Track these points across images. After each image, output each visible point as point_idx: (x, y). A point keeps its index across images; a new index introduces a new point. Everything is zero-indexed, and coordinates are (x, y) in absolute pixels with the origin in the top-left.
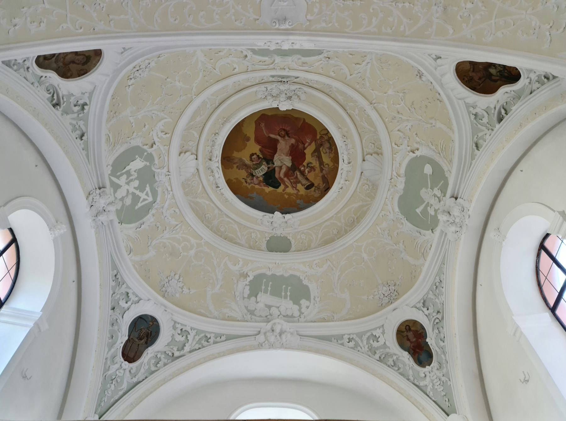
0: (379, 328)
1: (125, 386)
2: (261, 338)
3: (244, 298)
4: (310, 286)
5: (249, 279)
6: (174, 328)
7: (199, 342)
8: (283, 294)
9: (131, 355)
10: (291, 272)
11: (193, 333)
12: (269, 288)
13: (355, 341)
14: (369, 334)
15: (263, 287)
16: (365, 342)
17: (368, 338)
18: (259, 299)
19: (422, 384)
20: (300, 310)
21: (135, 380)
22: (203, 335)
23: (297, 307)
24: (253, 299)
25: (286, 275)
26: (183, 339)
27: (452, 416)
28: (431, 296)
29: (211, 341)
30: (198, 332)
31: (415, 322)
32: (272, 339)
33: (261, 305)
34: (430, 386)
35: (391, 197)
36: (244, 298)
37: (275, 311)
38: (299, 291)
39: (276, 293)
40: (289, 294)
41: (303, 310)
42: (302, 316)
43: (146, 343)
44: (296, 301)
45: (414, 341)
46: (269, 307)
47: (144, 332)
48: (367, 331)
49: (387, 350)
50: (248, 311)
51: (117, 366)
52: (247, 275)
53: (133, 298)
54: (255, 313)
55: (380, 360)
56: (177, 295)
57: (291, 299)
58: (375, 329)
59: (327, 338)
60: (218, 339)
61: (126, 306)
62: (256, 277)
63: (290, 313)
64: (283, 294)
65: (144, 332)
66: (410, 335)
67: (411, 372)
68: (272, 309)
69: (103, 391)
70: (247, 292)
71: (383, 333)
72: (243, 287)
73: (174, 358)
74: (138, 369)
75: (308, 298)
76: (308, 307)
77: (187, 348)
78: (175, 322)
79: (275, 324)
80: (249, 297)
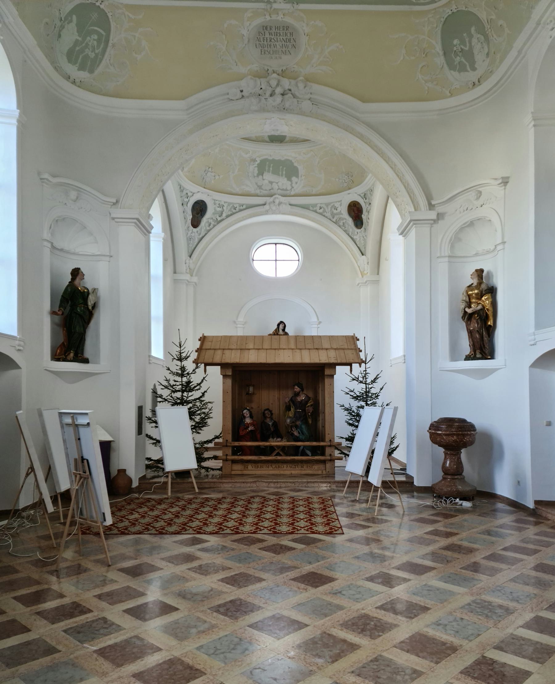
0: (339, 202)
1: (197, 241)
2: (267, 207)
3: (254, 177)
4: (298, 167)
5: (257, 163)
6: (215, 204)
7: (230, 210)
8: (280, 173)
9: (195, 224)
10: (286, 157)
11: (226, 205)
12: (271, 169)
13: (324, 208)
14: (332, 204)
15: (267, 168)
16: (329, 209)
17: (332, 206)
18: (264, 178)
19: (355, 237)
20: (291, 185)
21: (201, 236)
22: (231, 205)
23: (290, 183)
24: (260, 177)
25: (283, 159)
26: (221, 209)
27: (364, 256)
28: (368, 193)
29: (237, 209)
30: (229, 204)
31: (358, 203)
32: (274, 208)
33: (266, 182)
34: (358, 239)
35: (170, 670)
36: (254, 177)
37: (275, 186)
38: (289, 170)
39: (276, 172)
40: (284, 173)
41: (293, 185)
42: (293, 190)
43: (201, 215)
44: (289, 179)
45: (356, 212)
46: (271, 183)
47: (199, 209)
48: (332, 203)
49: (341, 216)
50: (258, 186)
51: (191, 232)
52: (255, 160)
53: (190, 194)
54: (263, 187)
55: (336, 223)
56: (213, 182)
57: (286, 177)
58: (337, 202)
59: (305, 207)
60: (241, 208)
61: (187, 200)
62: (261, 161)
63: (285, 188)
64: (280, 173)
65: (199, 209)
66: (355, 208)
67: (351, 230)
68: (274, 184)
69: (188, 244)
70: (256, 171)
71: (341, 205)
72: (253, 169)
73: (219, 222)
74: (201, 230)
75: (297, 176)
76: (296, 183)
77: (224, 215)
78: (215, 200)
79: (275, 198)
80: (258, 176)
